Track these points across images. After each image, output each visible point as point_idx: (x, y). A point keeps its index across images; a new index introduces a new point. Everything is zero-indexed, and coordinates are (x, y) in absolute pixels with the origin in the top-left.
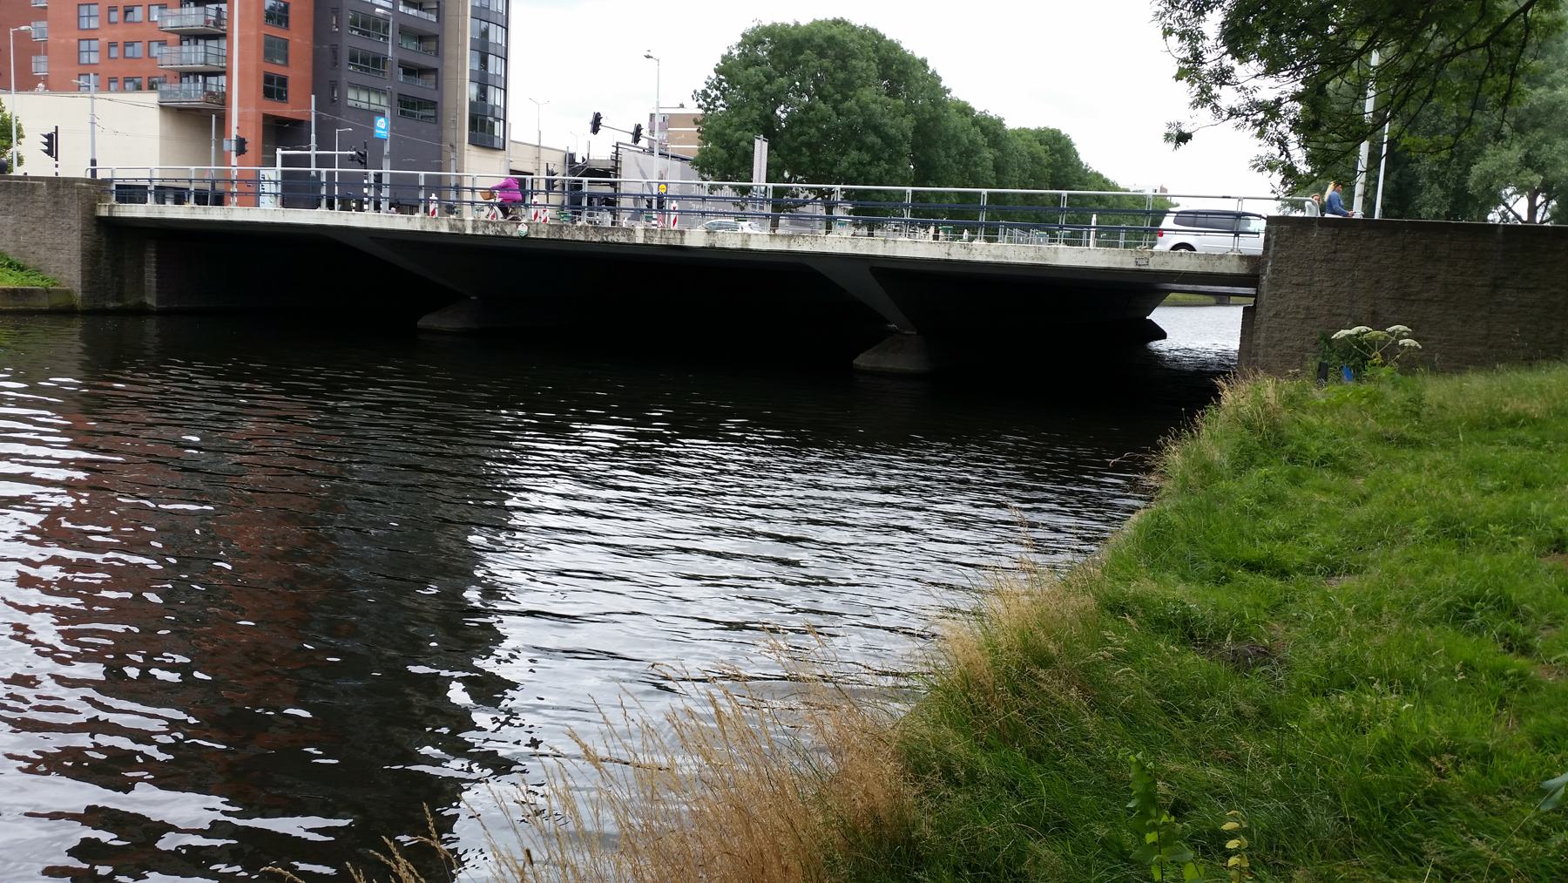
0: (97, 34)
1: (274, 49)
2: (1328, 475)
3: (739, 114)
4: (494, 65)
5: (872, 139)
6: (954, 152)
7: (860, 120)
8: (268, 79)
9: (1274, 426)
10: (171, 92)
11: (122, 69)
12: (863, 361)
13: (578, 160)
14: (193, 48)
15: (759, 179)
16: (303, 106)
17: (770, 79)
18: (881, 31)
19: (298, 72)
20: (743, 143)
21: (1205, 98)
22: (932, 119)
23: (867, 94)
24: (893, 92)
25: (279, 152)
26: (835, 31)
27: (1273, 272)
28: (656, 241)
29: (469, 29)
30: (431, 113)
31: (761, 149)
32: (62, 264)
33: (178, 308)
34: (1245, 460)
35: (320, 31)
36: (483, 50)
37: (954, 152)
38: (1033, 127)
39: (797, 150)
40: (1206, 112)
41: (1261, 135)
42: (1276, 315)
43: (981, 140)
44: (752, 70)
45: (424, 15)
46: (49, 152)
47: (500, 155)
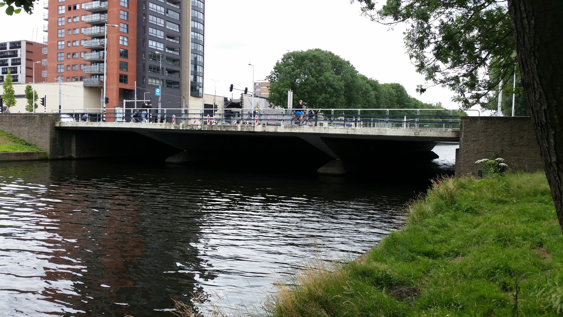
0: (63, 62)
1: (123, 66)
2: (469, 215)
3: (283, 82)
4: (199, 69)
5: (330, 89)
6: (360, 93)
8: (121, 76)
9: (452, 197)
10: (87, 81)
11: (71, 74)
12: (321, 170)
13: (229, 100)
14: (95, 66)
16: (132, 85)
17: (293, 70)
18: (333, 52)
19: (131, 73)
20: (285, 92)
21: (430, 76)
22: (352, 82)
23: (327, 74)
24: (337, 73)
25: (125, 101)
26: (316, 53)
27: (464, 136)
28: (245, 130)
29: (191, 57)
30: (177, 86)
31: (290, 94)
32: (43, 143)
33: (83, 159)
34: (438, 209)
35: (139, 59)
36: (195, 64)
37: (360, 93)
38: (389, 83)
39: (303, 94)
40: (431, 82)
41: (454, 89)
42: (467, 152)
43: (370, 88)
44: (287, 67)
45: (175, 53)
46: (43, 104)
47: (201, 99)
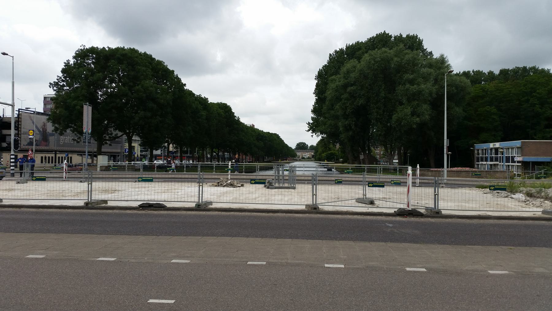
7: (144, 95)
15: (87, 125)
31: (87, 111)
